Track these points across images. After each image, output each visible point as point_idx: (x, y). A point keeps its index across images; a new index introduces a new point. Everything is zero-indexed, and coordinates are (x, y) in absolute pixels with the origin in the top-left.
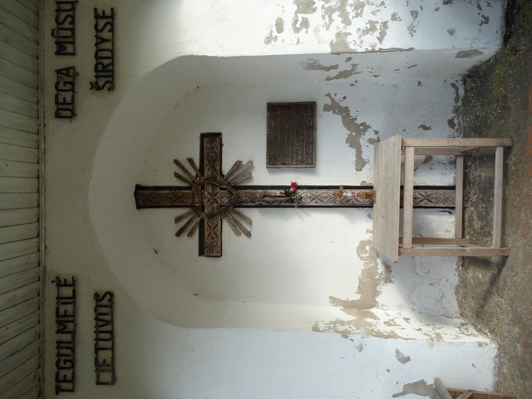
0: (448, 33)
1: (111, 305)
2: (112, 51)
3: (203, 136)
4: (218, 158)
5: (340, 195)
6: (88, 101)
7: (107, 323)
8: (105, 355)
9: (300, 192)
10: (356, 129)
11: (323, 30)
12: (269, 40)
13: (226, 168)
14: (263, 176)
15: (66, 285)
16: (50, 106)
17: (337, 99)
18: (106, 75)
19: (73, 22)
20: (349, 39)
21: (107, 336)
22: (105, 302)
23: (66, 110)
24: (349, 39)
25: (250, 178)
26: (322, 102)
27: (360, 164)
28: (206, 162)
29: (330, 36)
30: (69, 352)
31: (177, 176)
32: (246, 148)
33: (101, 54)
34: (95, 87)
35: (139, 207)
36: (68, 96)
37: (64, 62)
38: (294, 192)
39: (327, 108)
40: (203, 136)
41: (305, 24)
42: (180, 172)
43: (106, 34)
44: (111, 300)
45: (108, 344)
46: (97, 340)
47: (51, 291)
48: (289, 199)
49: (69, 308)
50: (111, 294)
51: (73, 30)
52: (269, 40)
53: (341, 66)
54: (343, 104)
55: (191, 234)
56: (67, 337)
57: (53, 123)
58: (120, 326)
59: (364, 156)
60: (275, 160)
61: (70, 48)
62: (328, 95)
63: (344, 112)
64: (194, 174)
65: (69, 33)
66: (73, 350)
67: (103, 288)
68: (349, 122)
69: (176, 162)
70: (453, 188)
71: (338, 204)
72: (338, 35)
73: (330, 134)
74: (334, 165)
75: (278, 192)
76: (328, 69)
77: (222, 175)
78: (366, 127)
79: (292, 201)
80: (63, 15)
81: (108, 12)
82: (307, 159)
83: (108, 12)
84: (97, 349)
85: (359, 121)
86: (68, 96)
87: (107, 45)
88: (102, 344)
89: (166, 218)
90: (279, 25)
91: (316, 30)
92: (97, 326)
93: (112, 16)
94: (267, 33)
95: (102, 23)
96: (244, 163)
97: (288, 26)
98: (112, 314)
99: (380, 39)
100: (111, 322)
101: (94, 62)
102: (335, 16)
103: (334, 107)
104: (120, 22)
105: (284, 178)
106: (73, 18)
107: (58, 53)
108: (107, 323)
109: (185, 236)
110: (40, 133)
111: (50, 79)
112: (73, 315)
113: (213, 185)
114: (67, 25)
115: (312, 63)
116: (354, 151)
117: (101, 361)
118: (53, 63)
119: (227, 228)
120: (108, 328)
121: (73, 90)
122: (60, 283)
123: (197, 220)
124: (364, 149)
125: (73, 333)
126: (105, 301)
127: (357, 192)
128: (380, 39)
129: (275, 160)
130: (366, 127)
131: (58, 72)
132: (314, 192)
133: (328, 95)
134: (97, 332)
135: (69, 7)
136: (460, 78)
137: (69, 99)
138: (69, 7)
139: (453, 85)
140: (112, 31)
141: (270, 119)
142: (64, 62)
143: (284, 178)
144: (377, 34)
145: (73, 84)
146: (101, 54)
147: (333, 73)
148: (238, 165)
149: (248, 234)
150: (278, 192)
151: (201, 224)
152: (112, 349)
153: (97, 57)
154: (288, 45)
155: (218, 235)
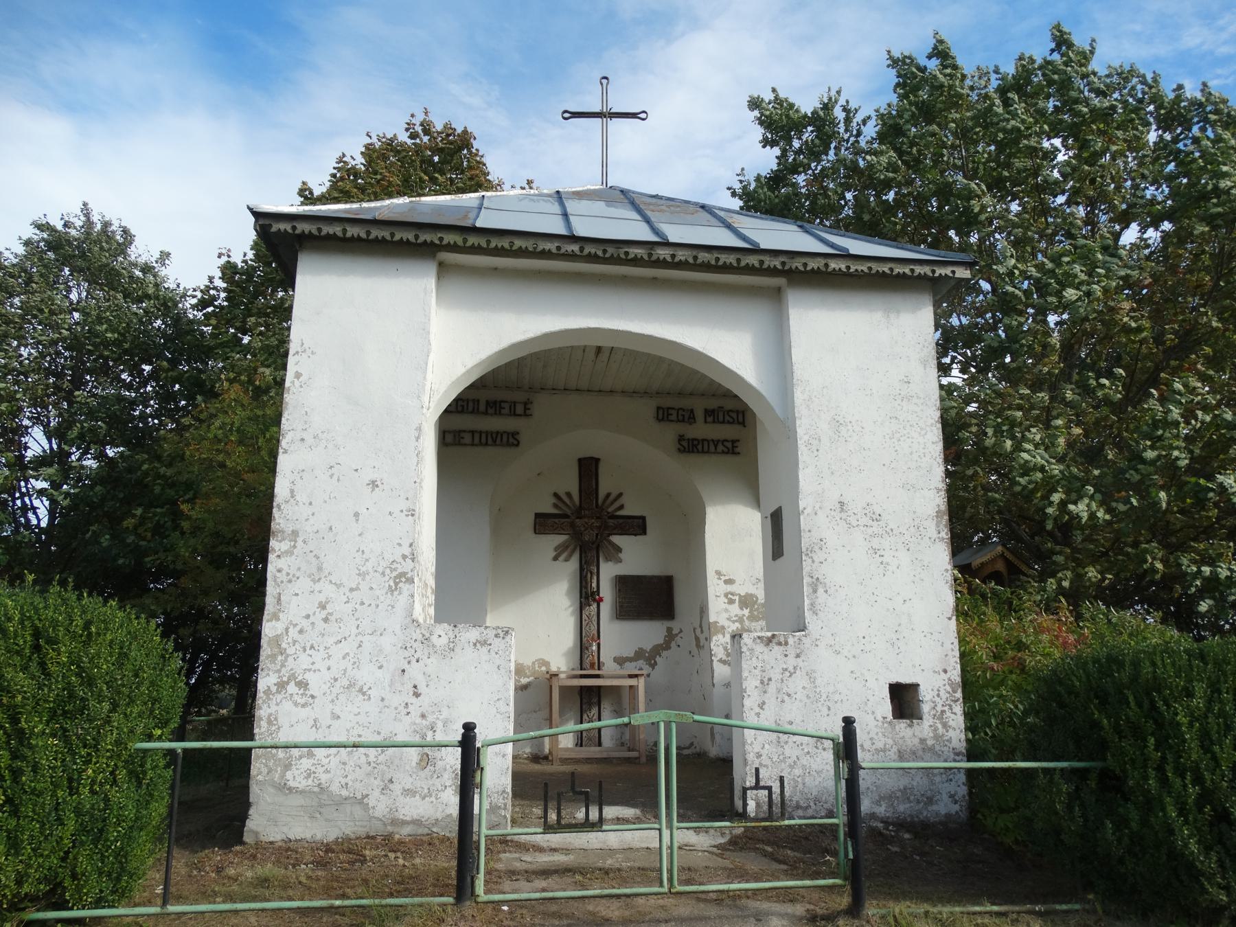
0: (588, 455)
1: (509, 444)
2: (708, 452)
3: (643, 518)
4: (624, 531)
5: (593, 640)
6: (670, 432)
7: (494, 441)
8: (467, 438)
9: (595, 605)
10: (650, 657)
11: (726, 615)
12: (718, 573)
13: (616, 539)
14: (608, 572)
15: (526, 409)
16: (669, 402)
17: (678, 638)
18: (690, 447)
19: (729, 422)
20: (720, 636)
21: (483, 440)
22: (511, 440)
23: (663, 415)
24: (720, 636)
25: (607, 560)
26: (675, 625)
27: (620, 661)
28: (621, 521)
29: (722, 621)
30: (470, 409)
31: (608, 495)
32: (634, 557)
33: (706, 444)
34: (681, 438)
35: (580, 460)
36: (674, 417)
37: (699, 414)
38: (594, 600)
39: (669, 630)
40: (643, 518)
41: (731, 602)
42: (612, 498)
43: (720, 448)
44: (513, 445)
45: (477, 440)
46: (481, 432)
47: (520, 396)
48: (587, 596)
49: (506, 411)
50: (517, 445)
51: (723, 422)
52: (718, 573)
53: (702, 631)
54: (673, 644)
55: (555, 506)
56: (482, 407)
57: (652, 404)
58: (491, 451)
59: (627, 664)
60: (624, 583)
61: (710, 419)
62: (681, 631)
63: (666, 646)
64: (610, 510)
65: (721, 419)
66: (472, 412)
67: (523, 438)
68: (657, 650)
69: (620, 495)
70: (600, 744)
71: (584, 640)
72: (723, 627)
73: (648, 633)
74: (619, 638)
75: (594, 585)
76: (701, 626)
77: (610, 535)
78: (653, 666)
79: (587, 598)
80: (734, 415)
81: (737, 450)
82: (625, 612)
83: (737, 450)
84: (473, 432)
85: (658, 659)
86: (674, 417)
87: (712, 448)
88: (477, 436)
89: (570, 484)
90: (729, 582)
91: (726, 610)
92: (492, 433)
93: (734, 453)
94: (724, 572)
95: (729, 445)
96: (620, 555)
97: (729, 588)
98: (502, 445)
99: (721, 661)
100: (494, 443)
101: (700, 438)
102: (737, 625)
103: (670, 636)
104: (729, 459)
105: (607, 591)
106: (733, 423)
107: (706, 411)
108: (494, 441)
109: (554, 500)
110: (646, 394)
111: (686, 403)
112: (500, 414)
113: (599, 528)
114: (727, 418)
115: (703, 610)
116: (632, 655)
117: (463, 435)
118: (699, 406)
119: (561, 539)
120: (490, 441)
121: (678, 421)
122: (527, 405)
123: (569, 512)
124: (634, 664)
125: (486, 413)
126: (511, 440)
127: (595, 654)
128: (721, 661)
129: (624, 583)
130: (653, 666)
131: (692, 411)
132: (595, 618)
133: (681, 631)
134: (487, 433)
135: (741, 419)
136: (698, 750)
137: (671, 418)
138: (741, 419)
139: (692, 744)
140: (723, 452)
141: (659, 578)
142: (699, 414)
143: (607, 591)
144: (724, 658)
145: (683, 421)
146: (706, 444)
147: (698, 631)
148: (619, 550)
149: (555, 559)
150: (594, 585)
151: (565, 516)
152: (472, 445)
153: (703, 440)
154: (715, 588)
155: (555, 530)
